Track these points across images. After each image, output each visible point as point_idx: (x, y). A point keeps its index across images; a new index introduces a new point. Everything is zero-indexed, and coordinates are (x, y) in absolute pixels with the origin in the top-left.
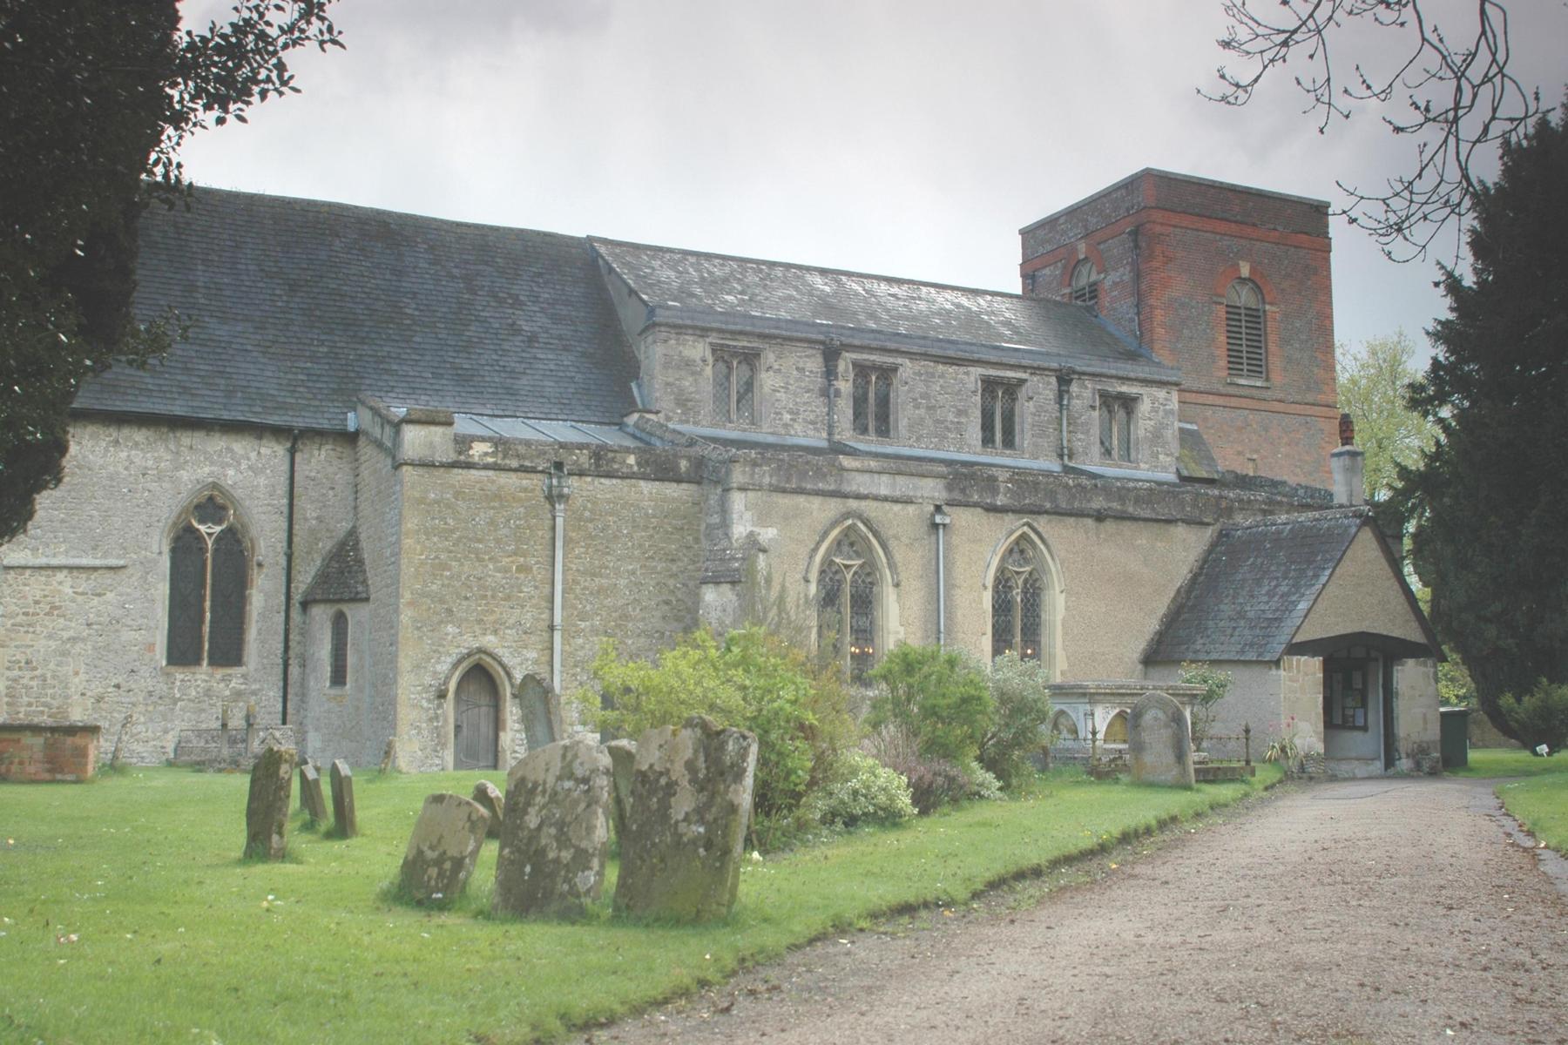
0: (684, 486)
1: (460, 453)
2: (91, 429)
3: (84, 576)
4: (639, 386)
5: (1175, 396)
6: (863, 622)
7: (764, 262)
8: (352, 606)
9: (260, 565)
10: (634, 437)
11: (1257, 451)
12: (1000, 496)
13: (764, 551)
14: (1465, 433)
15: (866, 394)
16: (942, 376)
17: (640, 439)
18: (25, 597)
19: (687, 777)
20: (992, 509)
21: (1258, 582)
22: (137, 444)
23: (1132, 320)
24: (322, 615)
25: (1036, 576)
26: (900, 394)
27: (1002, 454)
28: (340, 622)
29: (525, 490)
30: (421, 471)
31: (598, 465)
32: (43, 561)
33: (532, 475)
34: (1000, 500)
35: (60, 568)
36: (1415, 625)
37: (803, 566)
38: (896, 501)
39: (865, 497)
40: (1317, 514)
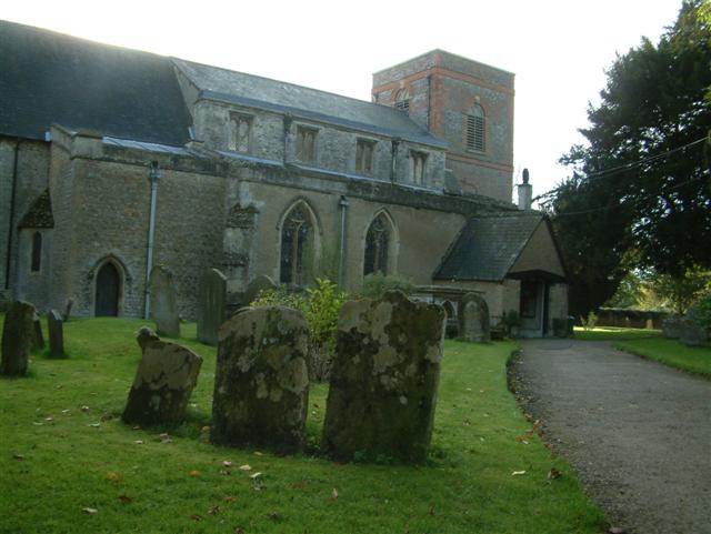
4: (193, 130)
20: (370, 200)
24: (27, 234)
26: (319, 143)
29: (138, 175)
34: (372, 196)
38: (323, 192)
39: (309, 189)
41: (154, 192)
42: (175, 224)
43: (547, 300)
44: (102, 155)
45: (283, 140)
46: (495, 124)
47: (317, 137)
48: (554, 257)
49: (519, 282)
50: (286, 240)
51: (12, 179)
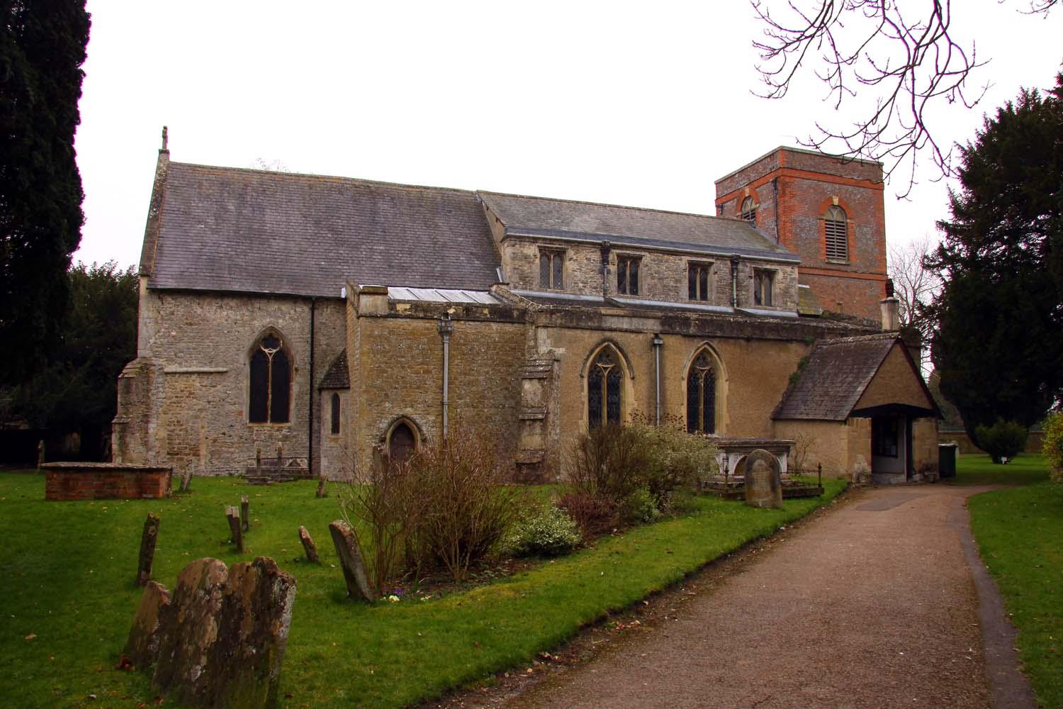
0: (516, 325)
1: (392, 310)
2: (208, 300)
3: (206, 377)
4: (501, 270)
5: (796, 270)
6: (615, 399)
7: (573, 202)
8: (341, 391)
9: (296, 370)
10: (494, 297)
11: (842, 299)
12: (692, 328)
13: (558, 361)
14: (953, 290)
15: (625, 271)
16: (667, 261)
17: (497, 299)
18: (176, 388)
19: (251, 606)
20: (685, 336)
21: (836, 375)
22: (231, 307)
23: (774, 229)
25: (712, 372)
26: (643, 271)
27: (700, 304)
28: (336, 401)
29: (428, 329)
30: (370, 320)
31: (467, 315)
32: (185, 369)
33: (432, 321)
34: (692, 330)
36: (925, 399)
37: (579, 369)
38: (632, 332)
39: (615, 330)
40: (870, 337)
41: (446, 346)
43: (910, 439)
45: (601, 272)
46: (859, 226)
47: (641, 265)
50: (594, 387)
51: (310, 340)
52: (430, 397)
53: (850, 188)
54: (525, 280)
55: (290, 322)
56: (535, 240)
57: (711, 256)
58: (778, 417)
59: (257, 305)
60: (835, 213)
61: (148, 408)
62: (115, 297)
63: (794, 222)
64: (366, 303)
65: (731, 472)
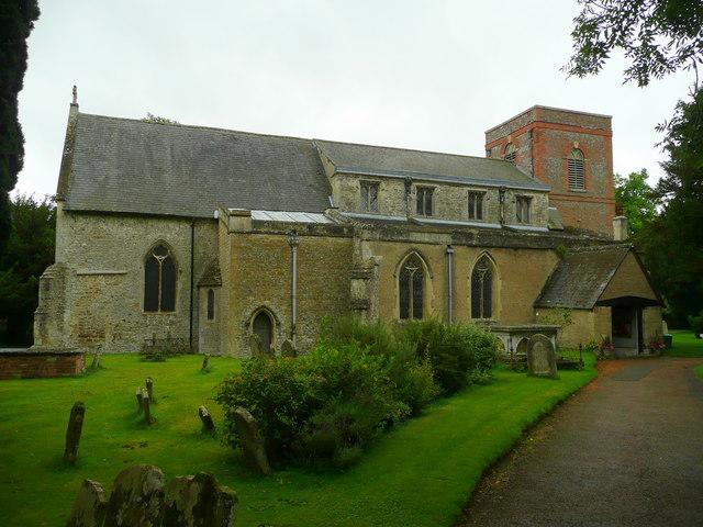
20: (470, 246)
24: (204, 292)
26: (435, 198)
28: (211, 294)
29: (281, 242)
32: (93, 272)
35: (101, 275)
37: (393, 272)
42: (314, 278)
44: (250, 229)
48: (644, 283)
49: (609, 308)
50: (403, 284)
52: (282, 292)
53: (587, 136)
54: (350, 205)
55: (176, 235)
56: (357, 176)
57: (484, 187)
58: (538, 306)
59: (150, 223)
60: (576, 154)
61: (64, 301)
62: (38, 221)
63: (546, 161)
64: (235, 222)
65: (515, 351)
